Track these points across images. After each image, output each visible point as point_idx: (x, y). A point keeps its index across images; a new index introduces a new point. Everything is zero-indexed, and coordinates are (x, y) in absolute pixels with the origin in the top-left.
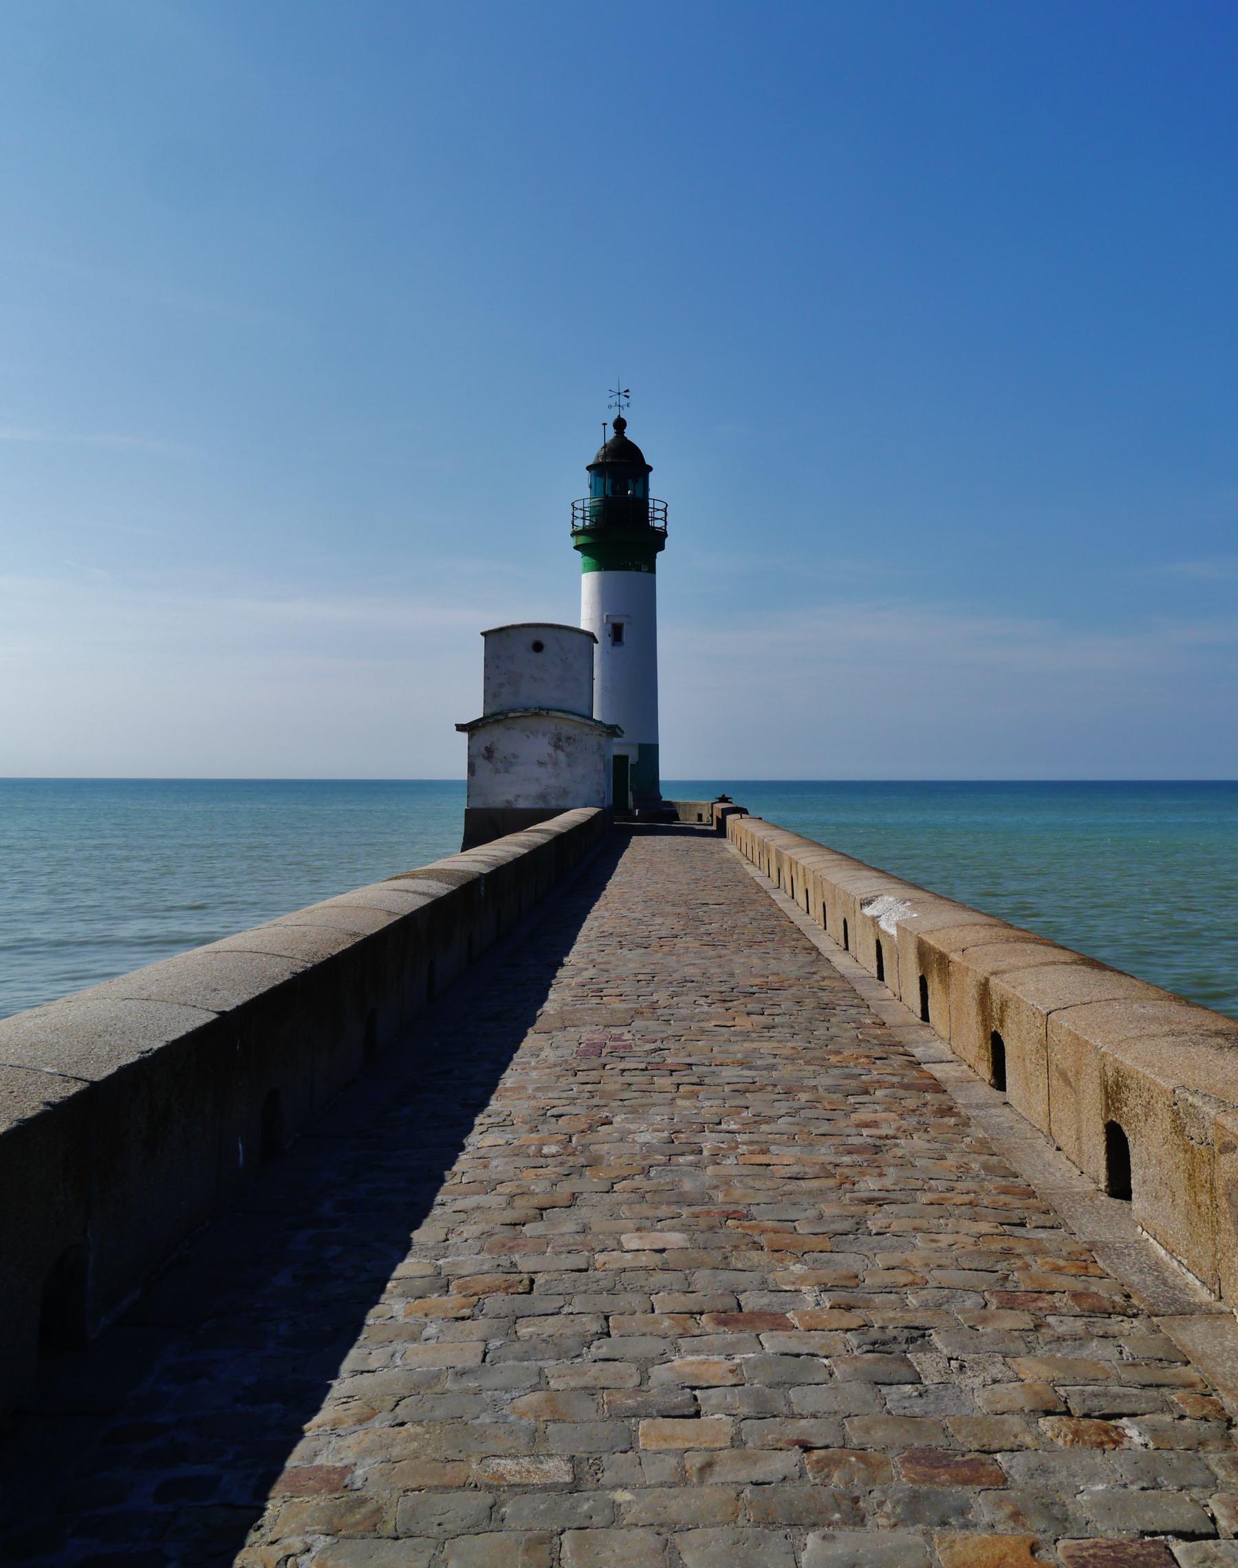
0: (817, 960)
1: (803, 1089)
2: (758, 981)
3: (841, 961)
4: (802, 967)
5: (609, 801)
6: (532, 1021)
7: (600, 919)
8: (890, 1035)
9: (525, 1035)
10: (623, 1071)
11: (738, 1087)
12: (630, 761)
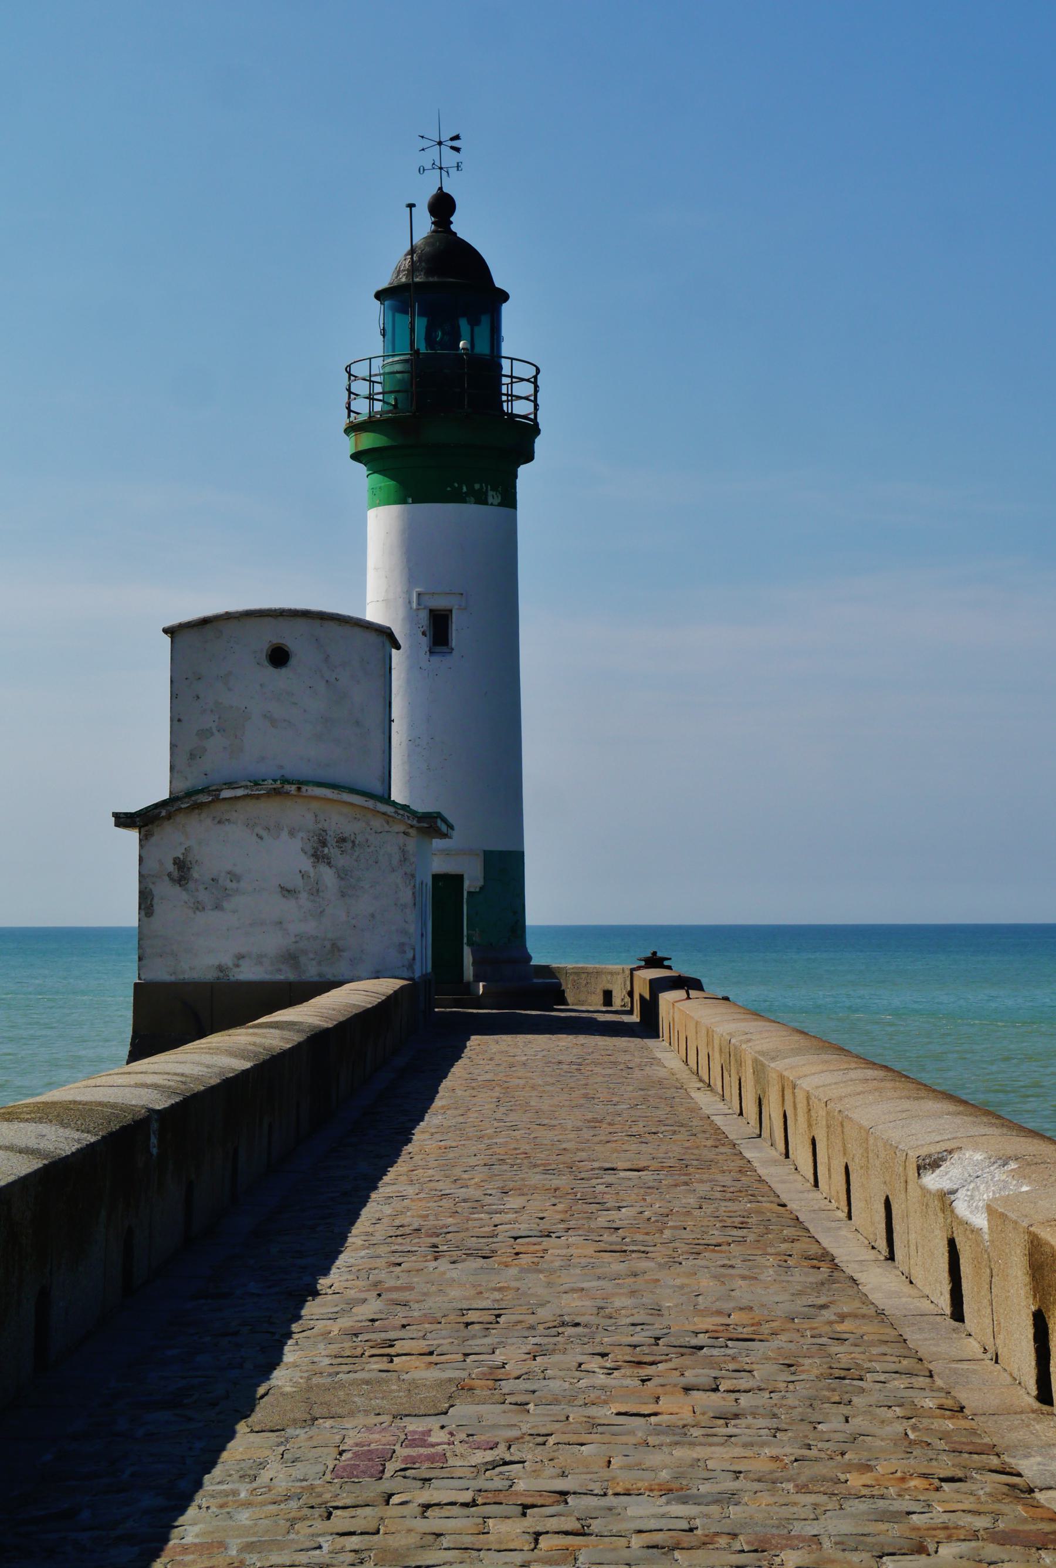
0: (831, 1280)
1: (791, 1542)
2: (708, 1323)
3: (878, 1282)
4: (800, 1293)
5: (424, 966)
6: (246, 1407)
7: (396, 1199)
8: (973, 1432)
9: (231, 1435)
10: (427, 1507)
11: (658, 1538)
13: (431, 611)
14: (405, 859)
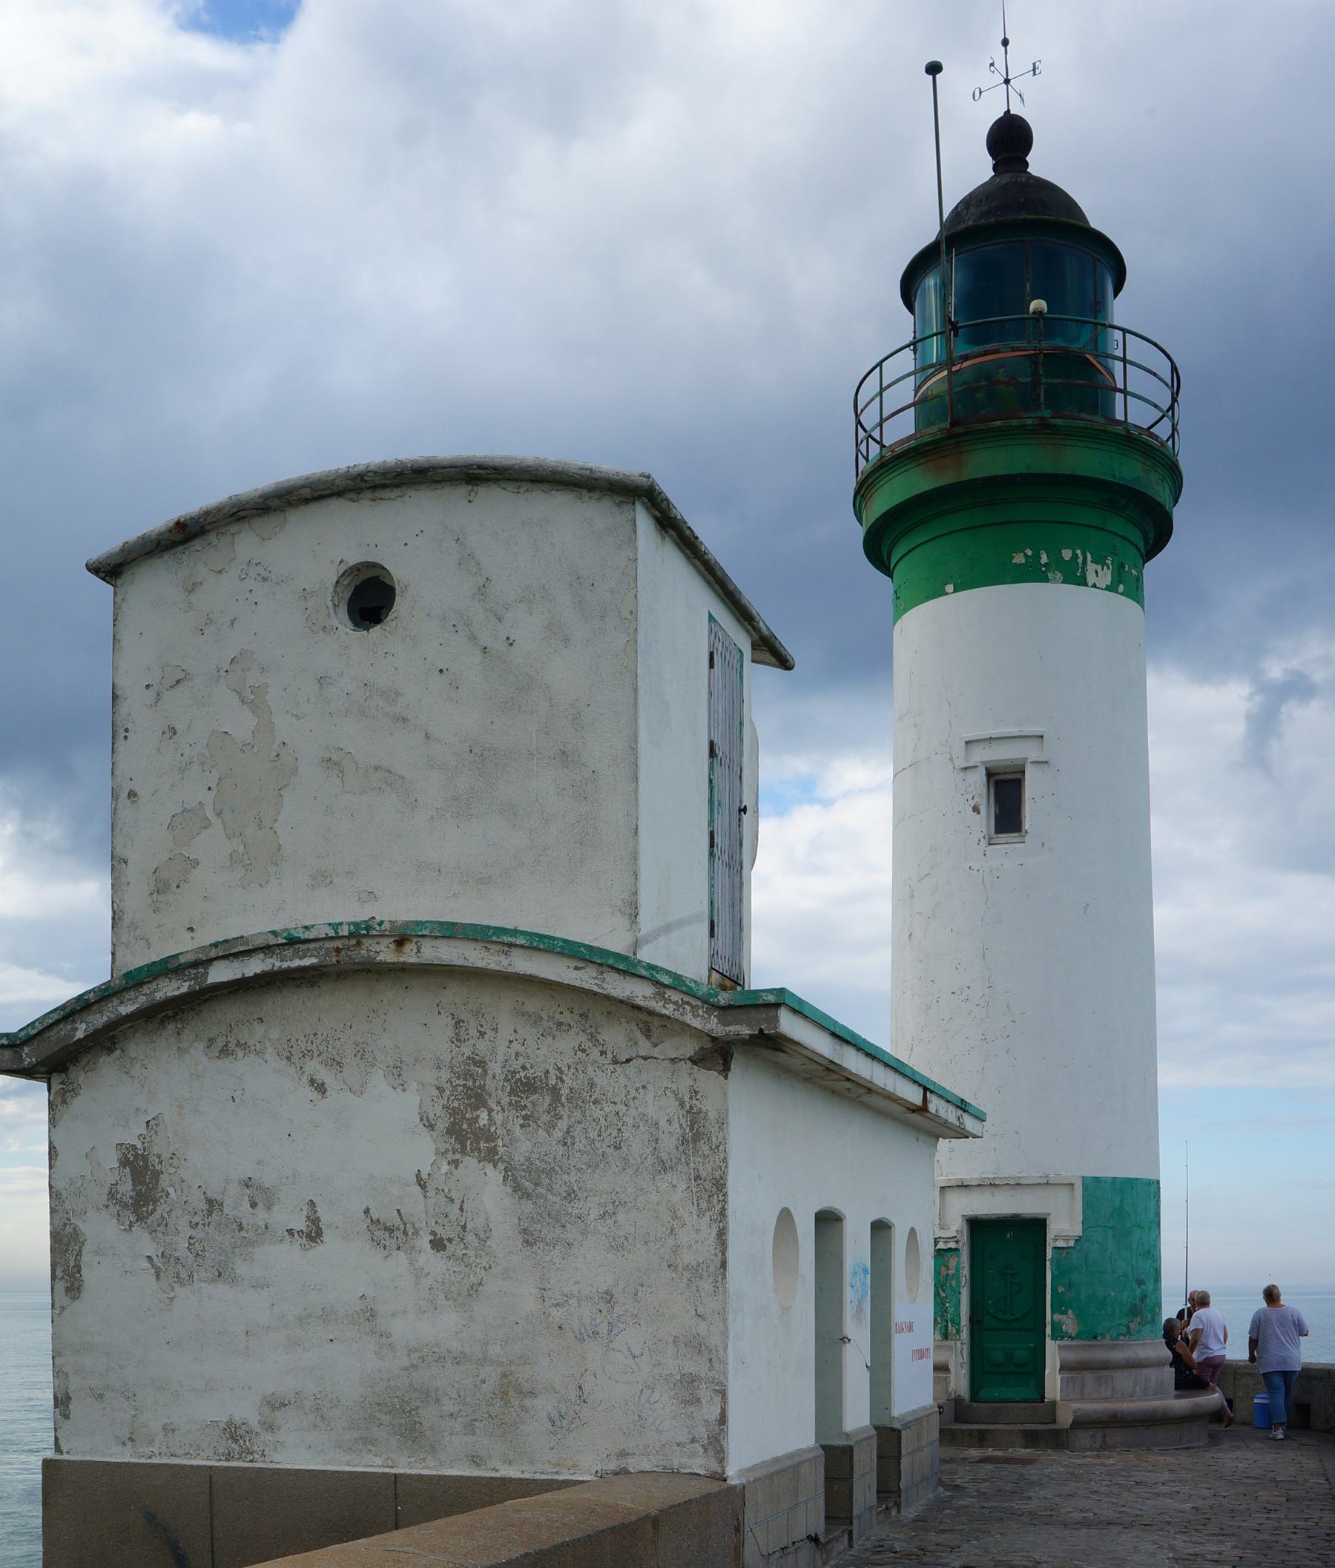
12: (1053, 1229)
13: (990, 774)
14: (696, 1138)
